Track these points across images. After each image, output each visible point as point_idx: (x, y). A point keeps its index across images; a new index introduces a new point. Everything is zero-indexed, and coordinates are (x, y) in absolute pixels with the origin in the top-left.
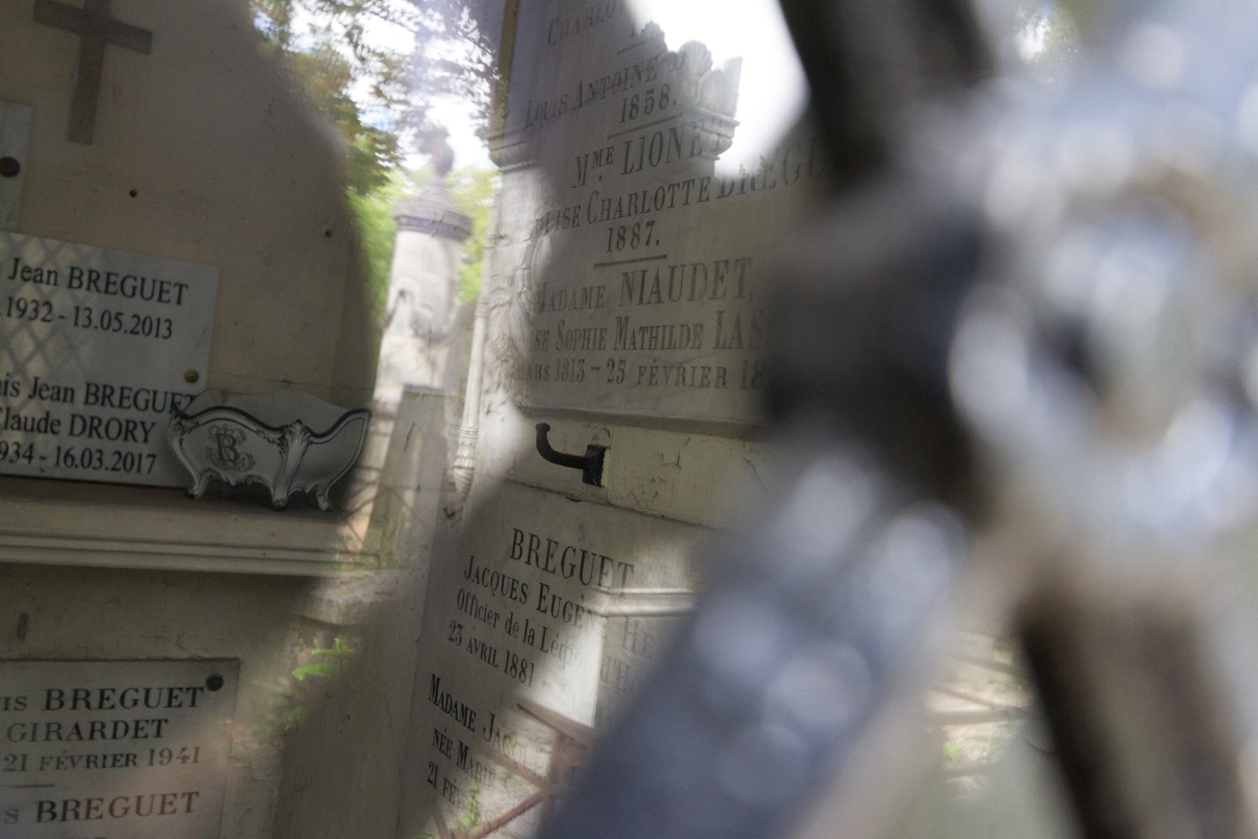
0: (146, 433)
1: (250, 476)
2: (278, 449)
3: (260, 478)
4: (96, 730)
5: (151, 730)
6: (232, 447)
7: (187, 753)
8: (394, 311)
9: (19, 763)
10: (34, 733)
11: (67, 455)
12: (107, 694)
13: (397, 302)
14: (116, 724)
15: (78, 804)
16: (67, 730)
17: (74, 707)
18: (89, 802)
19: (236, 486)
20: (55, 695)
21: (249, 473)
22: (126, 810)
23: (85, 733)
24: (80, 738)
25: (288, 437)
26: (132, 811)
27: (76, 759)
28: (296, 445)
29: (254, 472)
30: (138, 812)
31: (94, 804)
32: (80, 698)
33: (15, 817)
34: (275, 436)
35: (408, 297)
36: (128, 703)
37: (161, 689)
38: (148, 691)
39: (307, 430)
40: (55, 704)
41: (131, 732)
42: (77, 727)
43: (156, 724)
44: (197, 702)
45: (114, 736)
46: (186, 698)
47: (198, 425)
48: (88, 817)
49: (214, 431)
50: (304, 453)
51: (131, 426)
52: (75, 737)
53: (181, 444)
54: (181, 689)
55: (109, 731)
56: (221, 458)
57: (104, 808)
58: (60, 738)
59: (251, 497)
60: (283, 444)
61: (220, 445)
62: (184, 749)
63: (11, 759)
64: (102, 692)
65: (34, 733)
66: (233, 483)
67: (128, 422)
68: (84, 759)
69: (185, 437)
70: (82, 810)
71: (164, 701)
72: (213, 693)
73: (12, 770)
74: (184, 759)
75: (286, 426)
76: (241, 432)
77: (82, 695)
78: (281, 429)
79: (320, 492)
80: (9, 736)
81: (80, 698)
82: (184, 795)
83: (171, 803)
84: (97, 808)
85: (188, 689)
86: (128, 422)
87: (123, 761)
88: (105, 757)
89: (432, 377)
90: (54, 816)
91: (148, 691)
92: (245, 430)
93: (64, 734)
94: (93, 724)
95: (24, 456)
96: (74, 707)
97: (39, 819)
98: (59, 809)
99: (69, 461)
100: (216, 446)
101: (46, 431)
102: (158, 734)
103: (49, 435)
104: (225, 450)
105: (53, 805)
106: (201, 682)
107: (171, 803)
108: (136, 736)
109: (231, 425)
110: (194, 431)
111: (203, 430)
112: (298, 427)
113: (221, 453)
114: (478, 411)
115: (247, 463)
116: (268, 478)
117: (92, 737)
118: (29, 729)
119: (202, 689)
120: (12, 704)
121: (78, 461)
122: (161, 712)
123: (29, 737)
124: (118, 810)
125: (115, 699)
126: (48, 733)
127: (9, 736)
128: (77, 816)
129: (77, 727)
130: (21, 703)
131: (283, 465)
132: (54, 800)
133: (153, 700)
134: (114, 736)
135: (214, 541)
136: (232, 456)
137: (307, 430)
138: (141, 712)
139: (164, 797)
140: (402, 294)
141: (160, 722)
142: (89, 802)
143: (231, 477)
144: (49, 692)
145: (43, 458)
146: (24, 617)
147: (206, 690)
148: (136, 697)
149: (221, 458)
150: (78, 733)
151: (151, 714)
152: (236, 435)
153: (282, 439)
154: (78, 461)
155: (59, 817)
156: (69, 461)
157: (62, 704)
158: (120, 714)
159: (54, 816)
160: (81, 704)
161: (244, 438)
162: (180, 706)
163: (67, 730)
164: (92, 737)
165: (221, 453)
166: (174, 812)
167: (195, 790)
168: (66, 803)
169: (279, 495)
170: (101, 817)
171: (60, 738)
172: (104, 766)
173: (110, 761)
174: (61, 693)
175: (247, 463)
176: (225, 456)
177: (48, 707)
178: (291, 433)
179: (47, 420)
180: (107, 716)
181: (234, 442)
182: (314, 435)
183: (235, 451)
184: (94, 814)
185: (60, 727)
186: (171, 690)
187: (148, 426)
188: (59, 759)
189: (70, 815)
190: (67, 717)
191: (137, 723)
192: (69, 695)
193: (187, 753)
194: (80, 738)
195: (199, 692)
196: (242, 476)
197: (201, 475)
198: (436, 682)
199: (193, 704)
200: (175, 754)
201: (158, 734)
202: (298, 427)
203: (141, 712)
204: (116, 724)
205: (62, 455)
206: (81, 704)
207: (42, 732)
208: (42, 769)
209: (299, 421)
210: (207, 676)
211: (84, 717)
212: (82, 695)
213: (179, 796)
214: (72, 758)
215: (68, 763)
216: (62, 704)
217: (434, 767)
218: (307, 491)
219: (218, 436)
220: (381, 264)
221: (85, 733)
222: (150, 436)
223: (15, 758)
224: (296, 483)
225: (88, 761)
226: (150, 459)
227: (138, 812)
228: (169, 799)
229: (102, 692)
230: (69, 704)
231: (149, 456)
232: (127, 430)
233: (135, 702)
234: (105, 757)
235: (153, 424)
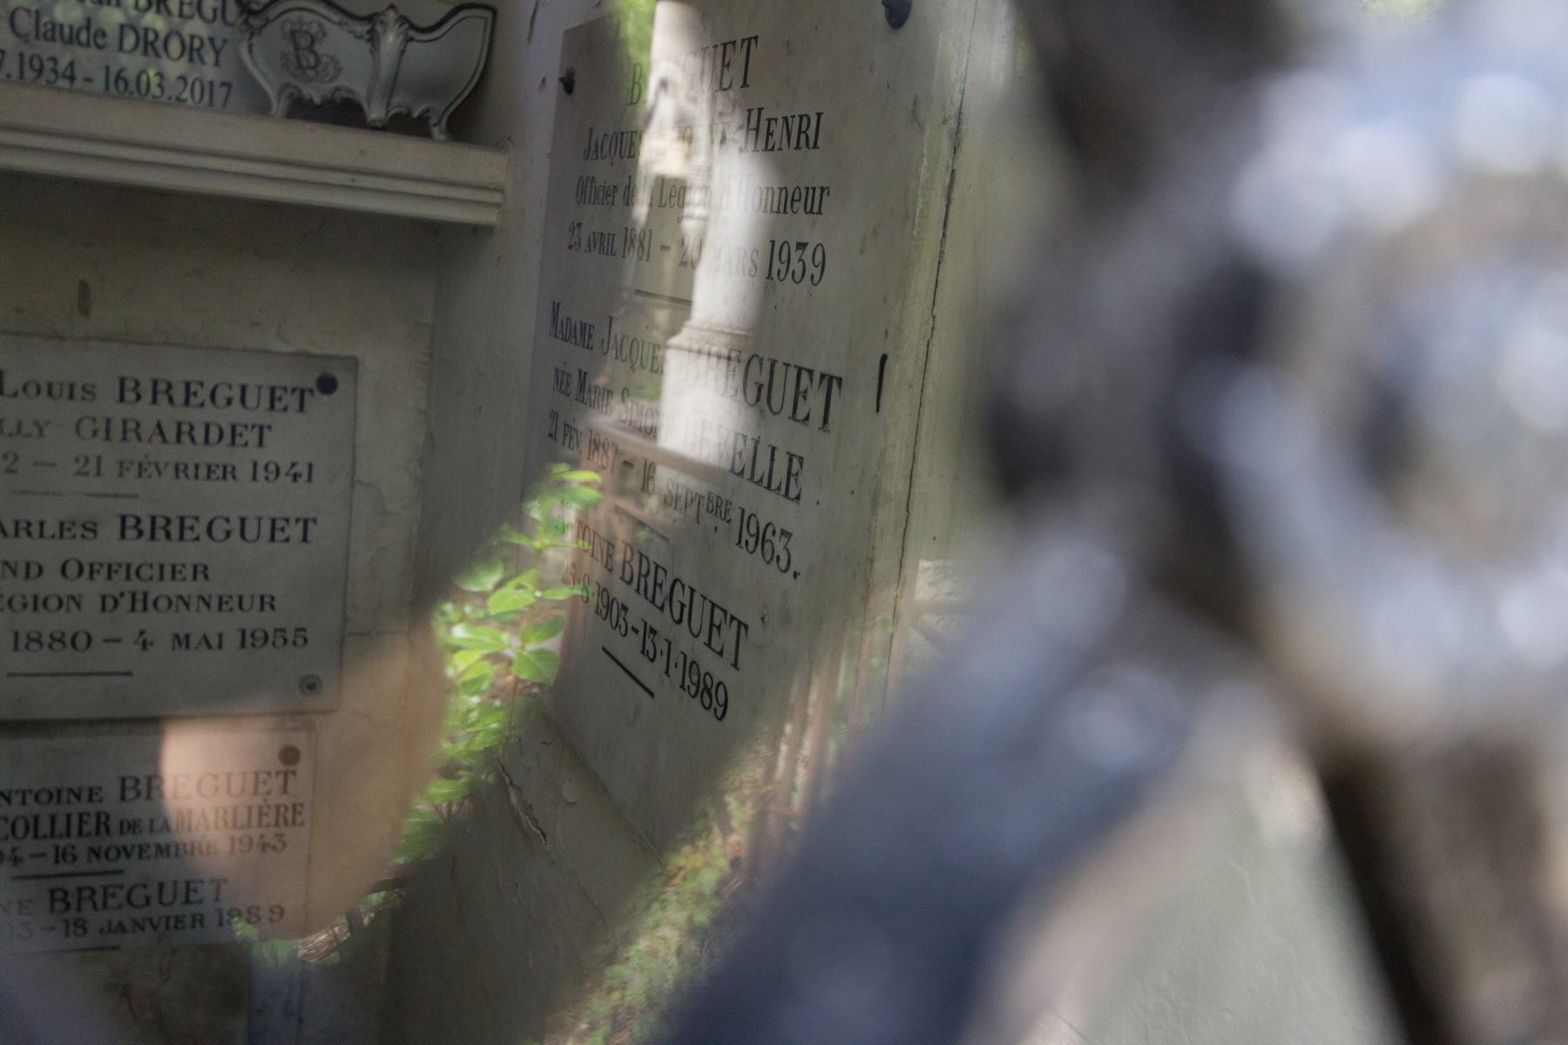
0: (217, 53)
1: (337, 89)
2: (368, 46)
3: (349, 90)
4: (183, 432)
5: (252, 437)
6: (311, 48)
7: (297, 469)
8: (654, 107)
9: (92, 466)
10: (108, 430)
11: (118, 77)
12: (193, 388)
13: (657, 95)
14: (207, 427)
15: (168, 521)
16: (147, 429)
17: (154, 401)
18: (182, 519)
19: (322, 105)
20: (129, 384)
21: (335, 84)
22: (228, 534)
23: (171, 434)
24: (165, 440)
25: (379, 28)
26: (236, 534)
27: (162, 466)
28: (391, 40)
29: (341, 82)
30: (243, 536)
31: (188, 523)
32: (160, 391)
33: (95, 532)
34: (362, 28)
35: (671, 89)
36: (220, 400)
37: (260, 388)
38: (243, 389)
39: (403, 20)
40: (130, 396)
41: (227, 438)
42: (159, 426)
43: (256, 430)
44: (306, 406)
45: (207, 441)
46: (292, 401)
47: (268, 22)
48: (181, 538)
49: (288, 27)
50: (403, 52)
51: (197, 43)
52: (158, 439)
53: (250, 51)
54: (285, 389)
55: (199, 434)
56: (300, 67)
57: (201, 529)
58: (139, 438)
59: (343, 112)
60: (373, 39)
61: (297, 48)
62: (293, 465)
63: (82, 461)
64: (188, 386)
65: (108, 430)
66: (317, 100)
67: (192, 37)
68: (171, 468)
69: (255, 40)
70: (174, 529)
71: (265, 403)
72: (325, 398)
73: (87, 474)
74: (295, 477)
75: (376, 15)
76: (320, 25)
77: (162, 387)
78: (370, 19)
79: (433, 121)
80: (78, 431)
81: (160, 391)
82: (297, 520)
83: (282, 529)
84: (192, 528)
85: (294, 390)
86: (192, 37)
87: (220, 472)
88: (197, 467)
89: (689, 156)
90: (140, 533)
91: (243, 389)
92: (325, 23)
93: (145, 434)
94: (179, 425)
95: (64, 76)
96: (154, 401)
97: (123, 536)
98: (146, 526)
99: (121, 85)
100: (290, 49)
101: (88, 45)
102: (261, 443)
103: (93, 50)
104: (303, 53)
105: (138, 521)
106: (311, 383)
107: (282, 529)
108: (233, 443)
109: (307, 17)
110: (265, 32)
111: (273, 29)
112: (391, 15)
113: (298, 59)
114: (712, 141)
115: (331, 68)
116: (360, 90)
117: (178, 440)
118: (101, 425)
119: (311, 391)
120: (78, 392)
121: (132, 86)
122: (261, 416)
123: (102, 434)
124: (218, 531)
125: (204, 394)
126: (125, 432)
127: (78, 431)
128: (168, 536)
129: (159, 426)
130: (89, 392)
131: (376, 67)
132: (139, 514)
133: (251, 399)
134: (207, 441)
135: (283, 156)
136: (312, 60)
137: (403, 20)
138: (236, 414)
139: (274, 521)
140: (664, 84)
141: (261, 428)
142: (182, 519)
143: (315, 93)
144: (122, 381)
145: (88, 80)
146: (84, 289)
147: (317, 393)
148: (229, 394)
149: (300, 67)
150: (162, 433)
151: (250, 417)
152: (314, 29)
153: (371, 31)
154: (132, 86)
155: (147, 533)
156: (121, 85)
157: (139, 397)
158: (209, 414)
159: (140, 533)
160: (162, 399)
161: (325, 35)
162: (285, 409)
163: (147, 429)
164: (178, 440)
165: (298, 59)
166: (287, 540)
167: (312, 515)
168: (153, 519)
169: (375, 113)
170: (197, 539)
171: (139, 438)
172: (196, 477)
173: (203, 472)
174: (137, 384)
175: (331, 68)
176: (304, 63)
177: (122, 398)
178: (382, 22)
179: (88, 28)
180: (198, 417)
181: (313, 42)
182: (413, 27)
183: (316, 54)
184: (188, 534)
185: (138, 425)
186: (273, 390)
187: (218, 44)
188: (140, 465)
189: (160, 534)
190: (146, 413)
191: (234, 428)
192: (146, 387)
193: (297, 469)
194: (165, 440)
195: (307, 395)
196: (327, 88)
197: (280, 93)
198: (556, 307)
199: (301, 408)
200: (283, 470)
201: (261, 443)
202: (391, 15)
203: (236, 414)
204: (207, 427)
205: (112, 79)
206: (162, 399)
207: (117, 429)
208: (121, 475)
209: (392, 7)
210: (316, 375)
211: (167, 414)
212: (162, 387)
213: (292, 521)
214: (157, 465)
215: (152, 470)
216: (139, 397)
217: (554, 416)
218: (416, 114)
219: (293, 33)
220: (633, 51)
221: (171, 434)
222: (223, 56)
223: (87, 460)
224: (397, 99)
225: (177, 469)
226: (225, 89)
227: (243, 536)
228: (279, 524)
229: (188, 386)
230: (147, 397)
231: (223, 84)
232: (192, 49)
233: (229, 402)
234: (197, 467)
235: (225, 41)
